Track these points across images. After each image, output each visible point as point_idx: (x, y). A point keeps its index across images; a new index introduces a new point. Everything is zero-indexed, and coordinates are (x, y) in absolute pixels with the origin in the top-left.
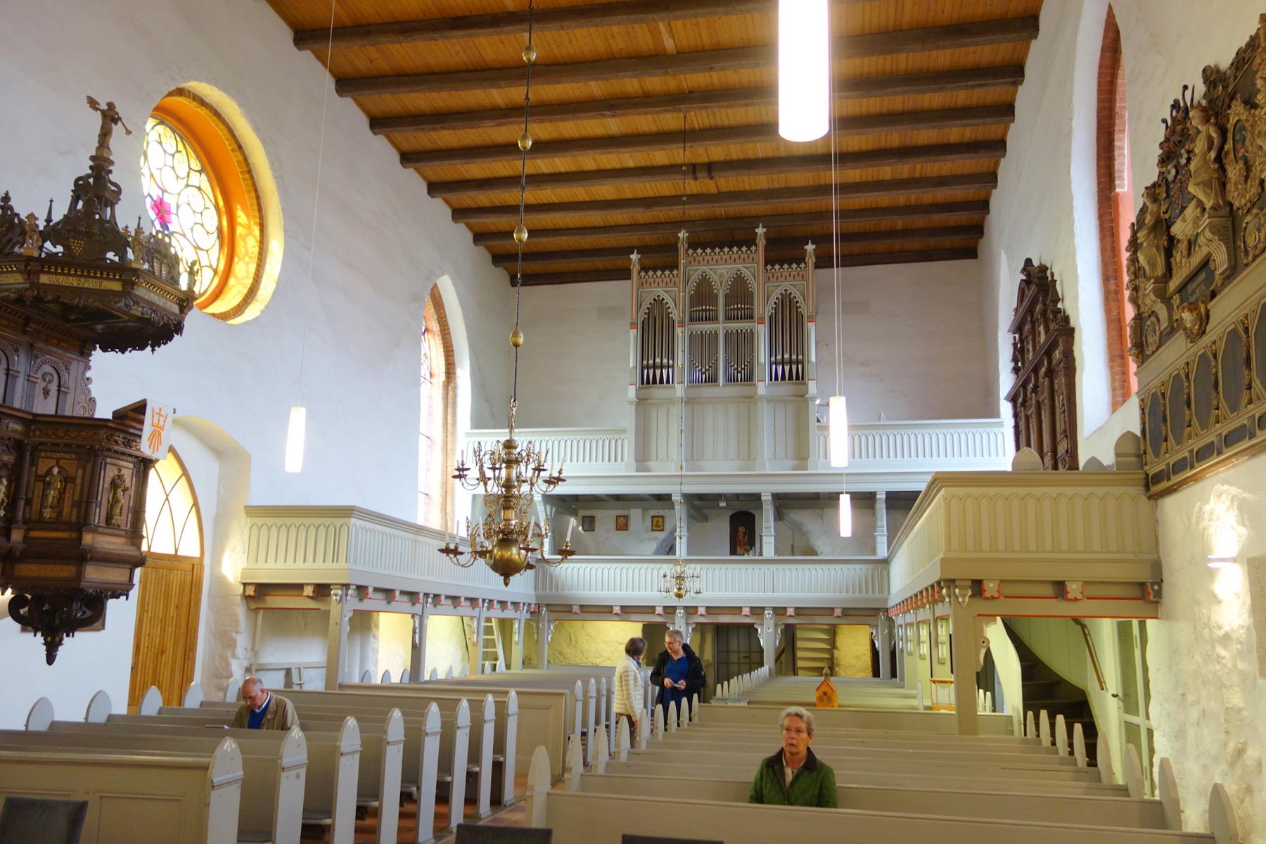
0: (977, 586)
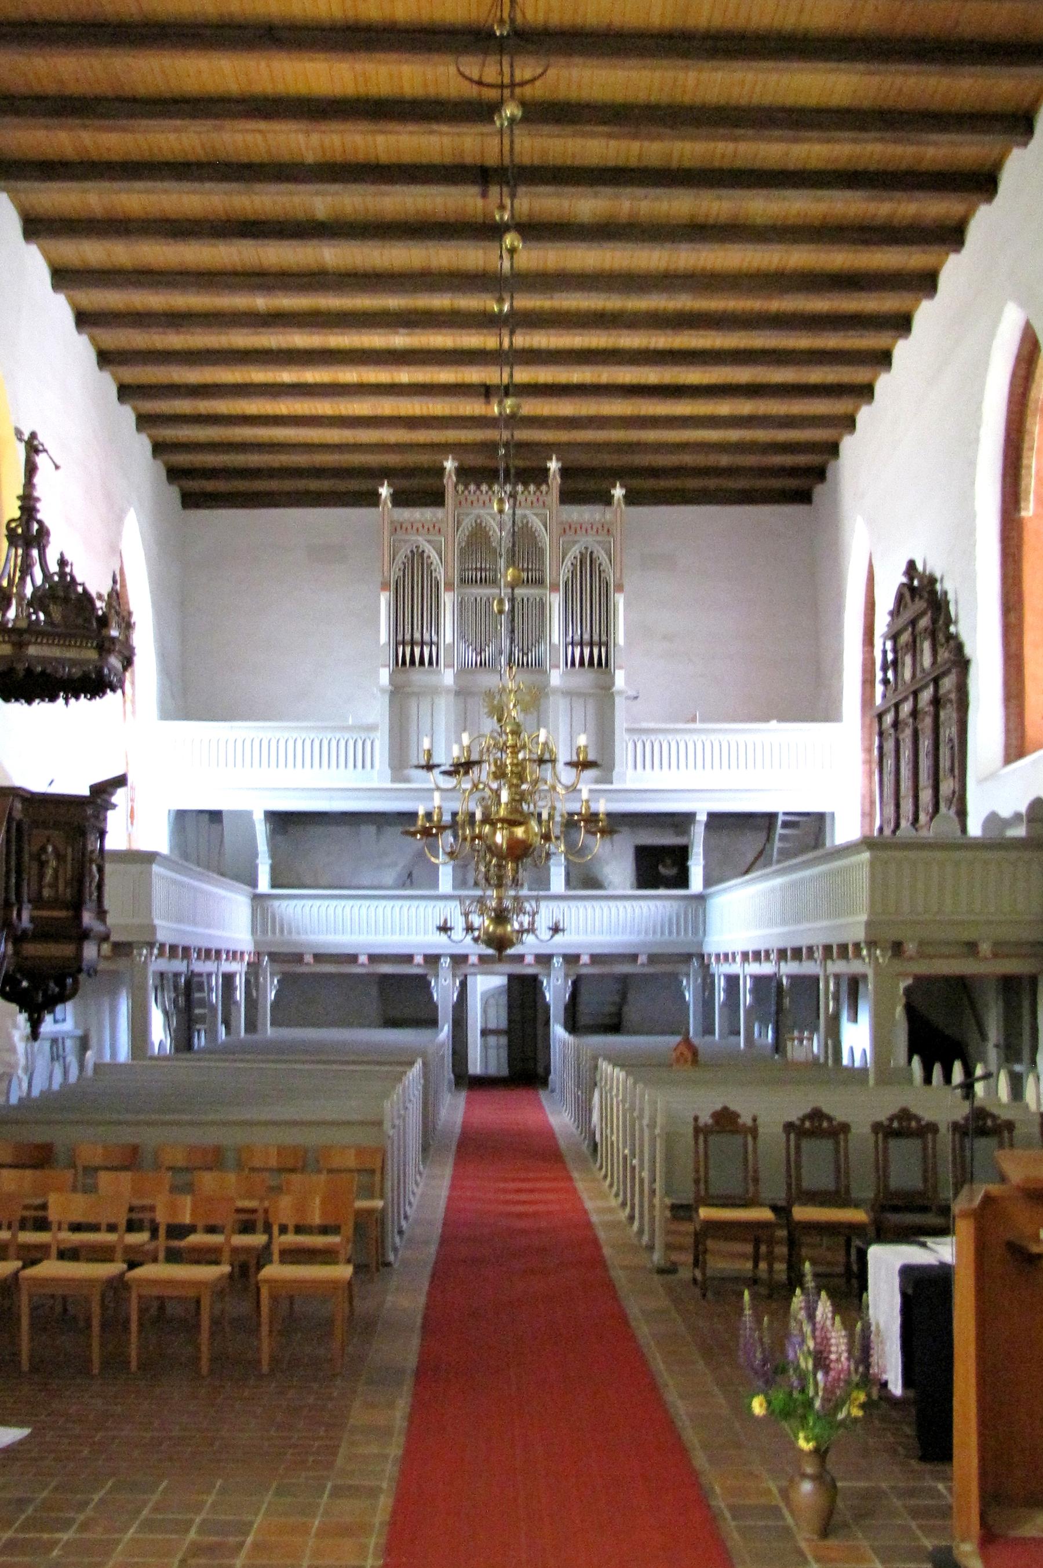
0: (897, 948)
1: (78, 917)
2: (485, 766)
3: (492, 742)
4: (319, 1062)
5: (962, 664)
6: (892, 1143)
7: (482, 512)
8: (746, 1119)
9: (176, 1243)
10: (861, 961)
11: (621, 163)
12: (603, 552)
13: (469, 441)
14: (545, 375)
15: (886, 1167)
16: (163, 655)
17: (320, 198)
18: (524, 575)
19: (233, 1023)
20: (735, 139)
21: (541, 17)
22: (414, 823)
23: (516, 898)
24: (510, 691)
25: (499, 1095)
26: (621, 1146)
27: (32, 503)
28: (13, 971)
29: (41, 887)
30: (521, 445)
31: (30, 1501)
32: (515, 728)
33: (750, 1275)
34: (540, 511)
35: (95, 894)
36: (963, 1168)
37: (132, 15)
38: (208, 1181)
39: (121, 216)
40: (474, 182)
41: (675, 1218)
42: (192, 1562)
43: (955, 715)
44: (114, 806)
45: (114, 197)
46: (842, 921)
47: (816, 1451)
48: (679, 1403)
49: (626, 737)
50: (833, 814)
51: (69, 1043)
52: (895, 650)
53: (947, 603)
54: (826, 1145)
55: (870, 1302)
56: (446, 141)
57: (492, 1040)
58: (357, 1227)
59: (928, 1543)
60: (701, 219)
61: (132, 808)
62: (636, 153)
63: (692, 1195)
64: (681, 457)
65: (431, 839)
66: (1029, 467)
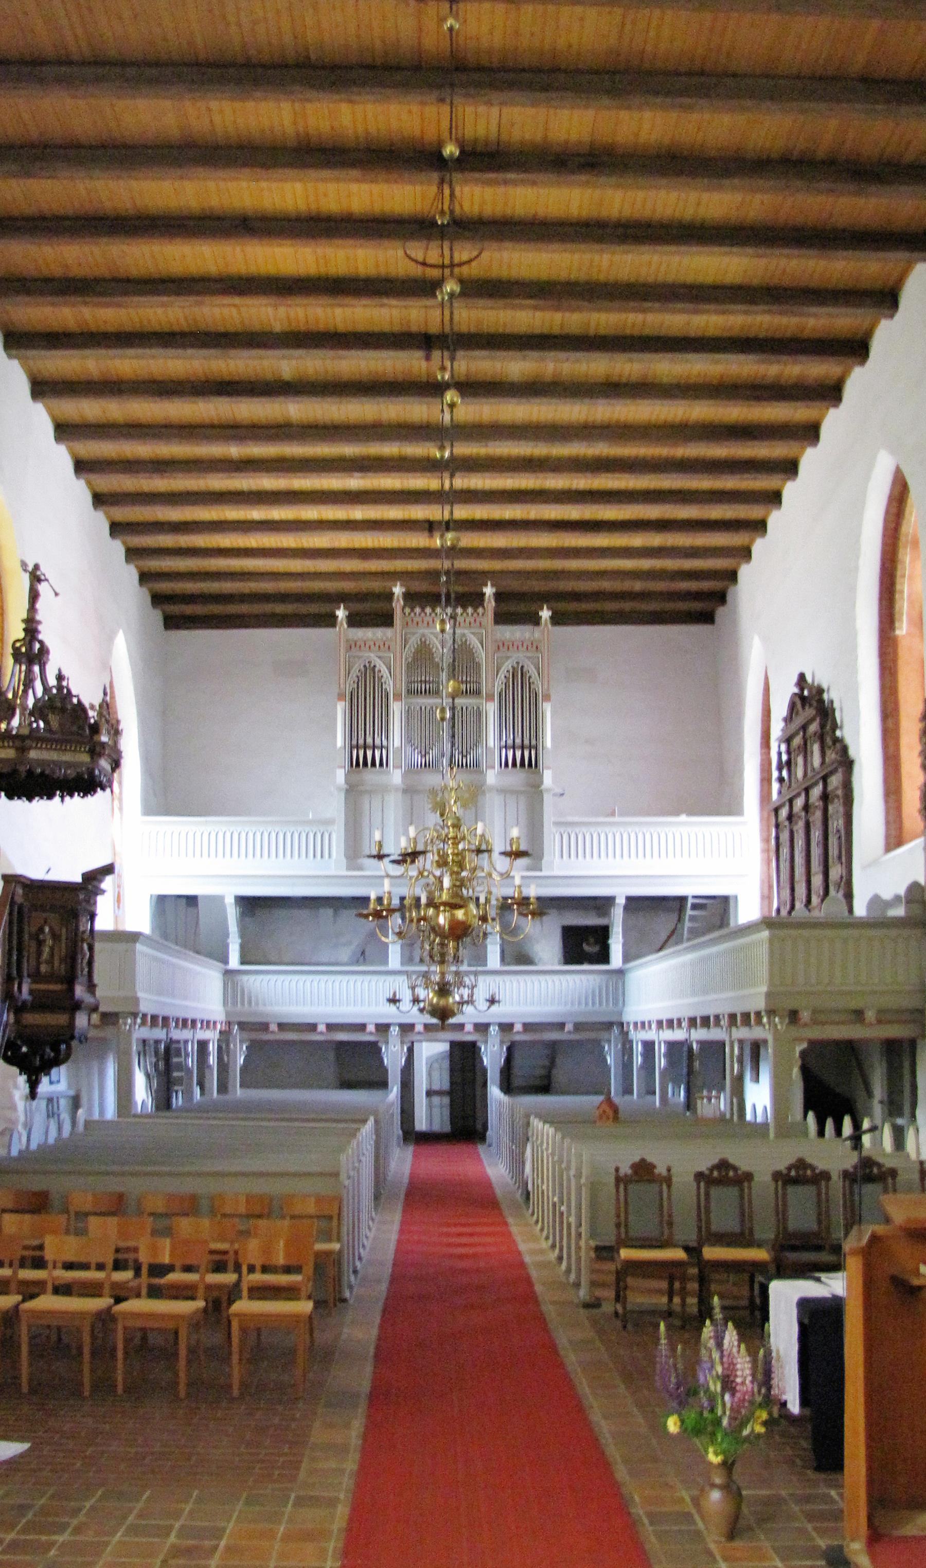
0: (794, 1016)
1: (71, 990)
2: (430, 856)
3: (435, 834)
4: (283, 1120)
5: (847, 764)
6: (791, 1189)
7: (426, 631)
8: (661, 1170)
9: (157, 1281)
10: (761, 1028)
11: (546, 331)
12: (532, 667)
13: (414, 570)
14: (480, 512)
15: (785, 1211)
16: (147, 758)
17: (286, 361)
18: (463, 687)
19: (207, 1085)
20: (644, 311)
21: (476, 210)
22: (367, 907)
23: (457, 973)
24: (451, 789)
25: (442, 1149)
26: (550, 1194)
27: (34, 625)
28: (15, 1038)
29: (39, 963)
30: (460, 573)
31: (30, 1507)
32: (456, 822)
33: (665, 1308)
34: (477, 631)
35: (86, 970)
36: (853, 1211)
37: (127, 210)
38: (185, 1225)
39: (115, 378)
40: (419, 348)
41: (599, 1258)
42: (172, 1562)
43: (841, 809)
44: (103, 892)
45: (109, 362)
46: (746, 992)
47: (724, 1463)
48: (603, 1423)
49: (554, 829)
50: (736, 897)
51: (63, 1102)
52: (789, 752)
53: (833, 710)
54: (732, 1192)
55: (771, 1332)
56: (395, 312)
57: (436, 1100)
58: (317, 1267)
59: (822, 1543)
60: (615, 379)
61: (119, 893)
62: (559, 323)
63: (613, 1238)
64: (599, 583)
65: (381, 920)
66: (902, 592)
